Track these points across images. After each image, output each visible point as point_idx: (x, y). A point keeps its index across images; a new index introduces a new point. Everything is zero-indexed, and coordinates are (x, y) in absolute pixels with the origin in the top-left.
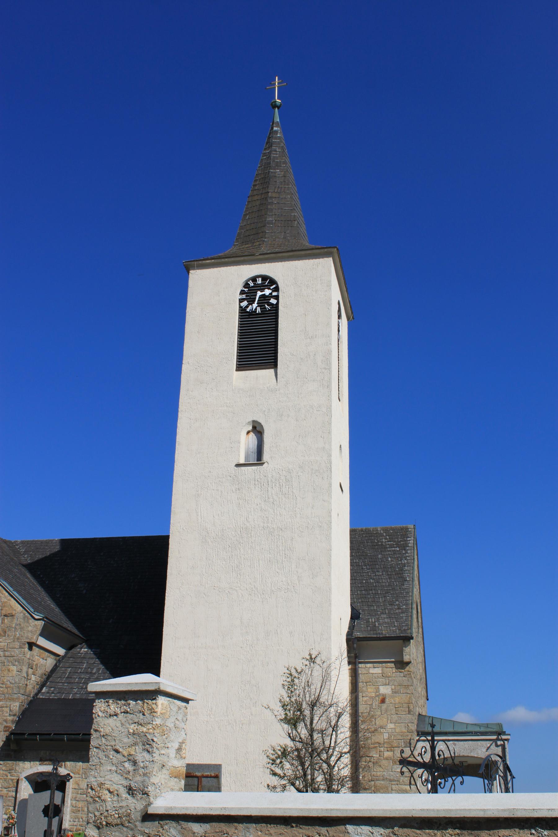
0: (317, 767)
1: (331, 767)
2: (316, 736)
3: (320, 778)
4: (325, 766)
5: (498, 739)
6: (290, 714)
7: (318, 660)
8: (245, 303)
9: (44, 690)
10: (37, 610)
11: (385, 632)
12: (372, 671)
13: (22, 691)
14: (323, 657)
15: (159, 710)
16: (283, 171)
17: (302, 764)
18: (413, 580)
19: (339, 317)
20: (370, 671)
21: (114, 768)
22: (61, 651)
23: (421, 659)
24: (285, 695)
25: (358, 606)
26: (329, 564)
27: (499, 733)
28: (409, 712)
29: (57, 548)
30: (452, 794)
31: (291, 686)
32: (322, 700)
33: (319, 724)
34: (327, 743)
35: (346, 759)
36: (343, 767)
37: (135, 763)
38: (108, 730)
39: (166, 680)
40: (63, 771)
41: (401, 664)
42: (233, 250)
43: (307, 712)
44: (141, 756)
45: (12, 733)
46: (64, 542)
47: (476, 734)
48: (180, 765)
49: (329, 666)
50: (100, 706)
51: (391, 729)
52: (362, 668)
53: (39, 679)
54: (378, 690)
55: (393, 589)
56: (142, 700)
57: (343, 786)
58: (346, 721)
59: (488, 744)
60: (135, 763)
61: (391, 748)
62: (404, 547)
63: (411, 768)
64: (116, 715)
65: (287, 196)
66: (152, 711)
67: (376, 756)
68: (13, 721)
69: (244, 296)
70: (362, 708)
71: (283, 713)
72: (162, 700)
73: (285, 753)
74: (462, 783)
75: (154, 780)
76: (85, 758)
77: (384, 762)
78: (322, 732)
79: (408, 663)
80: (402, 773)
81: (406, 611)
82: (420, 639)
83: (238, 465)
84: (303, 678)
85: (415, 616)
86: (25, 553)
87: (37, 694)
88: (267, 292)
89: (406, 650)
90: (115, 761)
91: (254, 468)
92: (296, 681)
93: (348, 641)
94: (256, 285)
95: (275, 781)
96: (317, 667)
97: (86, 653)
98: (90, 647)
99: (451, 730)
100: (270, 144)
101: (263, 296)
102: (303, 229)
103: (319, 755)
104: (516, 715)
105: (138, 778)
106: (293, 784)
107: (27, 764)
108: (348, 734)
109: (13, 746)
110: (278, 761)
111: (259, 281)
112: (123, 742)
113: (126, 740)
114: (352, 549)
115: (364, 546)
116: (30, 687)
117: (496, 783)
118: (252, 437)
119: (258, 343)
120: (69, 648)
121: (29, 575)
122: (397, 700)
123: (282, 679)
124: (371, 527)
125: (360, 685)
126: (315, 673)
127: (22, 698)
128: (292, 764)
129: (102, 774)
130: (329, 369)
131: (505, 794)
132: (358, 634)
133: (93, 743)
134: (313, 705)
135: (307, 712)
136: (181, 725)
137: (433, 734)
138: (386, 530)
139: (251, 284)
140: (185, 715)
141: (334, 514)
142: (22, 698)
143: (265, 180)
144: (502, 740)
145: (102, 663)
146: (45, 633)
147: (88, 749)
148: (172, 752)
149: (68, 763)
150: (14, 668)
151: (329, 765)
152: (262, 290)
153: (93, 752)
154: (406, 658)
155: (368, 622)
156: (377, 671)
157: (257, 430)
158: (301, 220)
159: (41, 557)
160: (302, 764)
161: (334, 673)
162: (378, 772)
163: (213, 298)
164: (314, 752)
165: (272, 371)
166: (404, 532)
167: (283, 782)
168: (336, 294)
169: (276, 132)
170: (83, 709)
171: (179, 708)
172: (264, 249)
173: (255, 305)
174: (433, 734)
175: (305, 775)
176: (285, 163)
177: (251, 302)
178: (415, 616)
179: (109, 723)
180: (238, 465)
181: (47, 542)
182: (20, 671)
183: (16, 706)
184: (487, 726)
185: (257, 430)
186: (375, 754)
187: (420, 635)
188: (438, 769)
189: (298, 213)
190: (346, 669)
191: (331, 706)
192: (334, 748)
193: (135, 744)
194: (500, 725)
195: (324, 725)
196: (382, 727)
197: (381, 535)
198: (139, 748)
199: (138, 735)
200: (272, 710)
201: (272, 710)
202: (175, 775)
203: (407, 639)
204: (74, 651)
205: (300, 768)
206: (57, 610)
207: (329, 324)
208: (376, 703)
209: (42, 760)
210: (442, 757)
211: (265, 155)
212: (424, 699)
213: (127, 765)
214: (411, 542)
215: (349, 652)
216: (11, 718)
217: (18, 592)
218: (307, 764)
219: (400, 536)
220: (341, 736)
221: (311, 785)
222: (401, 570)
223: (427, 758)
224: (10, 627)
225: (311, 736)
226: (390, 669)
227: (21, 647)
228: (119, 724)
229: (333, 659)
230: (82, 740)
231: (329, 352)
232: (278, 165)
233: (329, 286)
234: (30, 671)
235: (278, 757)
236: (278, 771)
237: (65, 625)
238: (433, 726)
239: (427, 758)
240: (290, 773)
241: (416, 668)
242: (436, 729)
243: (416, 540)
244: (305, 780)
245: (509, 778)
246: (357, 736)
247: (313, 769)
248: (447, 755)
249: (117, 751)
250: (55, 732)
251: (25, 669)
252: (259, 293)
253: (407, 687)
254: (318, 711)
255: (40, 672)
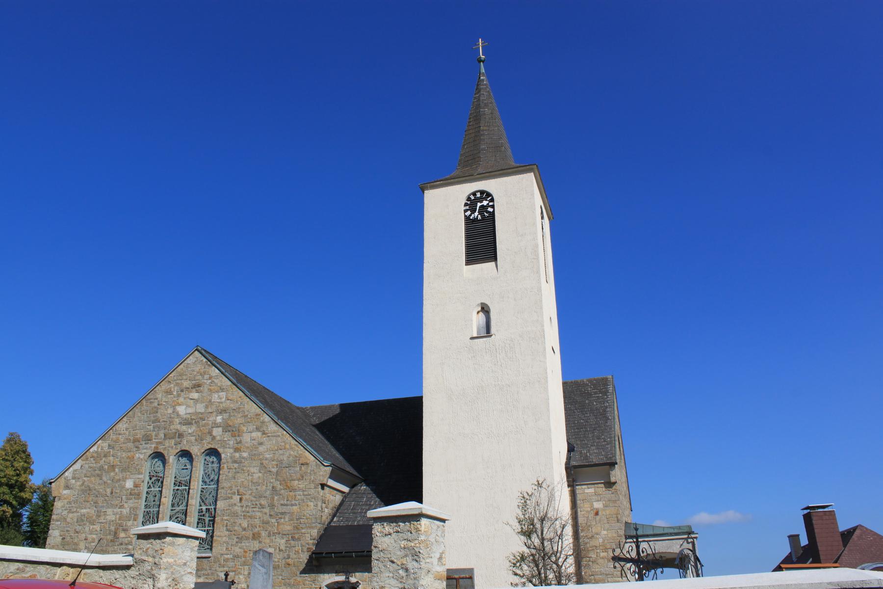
0: (548, 567)
1: (559, 567)
2: (546, 543)
3: (551, 576)
4: (554, 566)
5: (688, 538)
6: (525, 528)
7: (544, 485)
8: (469, 213)
9: (335, 519)
10: (325, 459)
11: (595, 460)
12: (587, 491)
13: (319, 521)
14: (548, 482)
15: (423, 529)
16: (491, 109)
17: (537, 566)
18: (614, 418)
19: (542, 218)
20: (586, 491)
21: (391, 575)
22: (346, 489)
23: (624, 479)
24: (520, 513)
25: (572, 441)
26: (548, 410)
27: (689, 533)
28: (618, 521)
29: (338, 411)
30: (655, 581)
31: (524, 506)
32: (549, 515)
33: (548, 534)
34: (555, 548)
35: (571, 560)
36: (569, 567)
37: (407, 570)
38: (385, 546)
39: (426, 507)
40: (353, 580)
41: (609, 484)
42: (455, 173)
43: (538, 526)
44: (411, 565)
45: (313, 553)
46: (343, 407)
47: (671, 534)
48: (442, 570)
49: (553, 489)
50: (377, 528)
51: (605, 535)
52: (579, 489)
53: (331, 511)
54: (592, 505)
55: (599, 427)
56: (409, 522)
57: (570, 581)
58: (569, 531)
59: (681, 542)
60: (407, 570)
61: (605, 550)
62: (606, 393)
63: (622, 563)
64: (390, 534)
65: (495, 127)
66: (418, 530)
67: (594, 556)
68: (313, 544)
69: (467, 207)
70: (581, 520)
71: (519, 527)
72: (424, 521)
73: (523, 558)
74: (662, 572)
75: (422, 582)
76: (369, 569)
77: (600, 561)
78: (551, 540)
79: (615, 483)
80: (615, 567)
81: (610, 442)
82: (623, 464)
83: (472, 338)
84: (534, 499)
85: (617, 446)
86: (314, 416)
87: (330, 523)
88: (485, 203)
89: (613, 473)
90: (391, 569)
91: (484, 339)
92: (528, 502)
93: (566, 469)
94: (476, 199)
95: (516, 579)
96: (543, 490)
97: (365, 490)
98: (367, 485)
99: (652, 533)
100: (478, 90)
101: (482, 206)
102: (509, 152)
103: (549, 558)
104: (700, 519)
105: (411, 582)
106: (531, 582)
107: (326, 576)
108: (571, 540)
109: (315, 563)
110: (518, 564)
111: (478, 195)
112: (397, 555)
113: (399, 553)
114: (565, 397)
115: (575, 395)
116: (324, 518)
117: (689, 572)
118: (482, 316)
119: (481, 242)
120: (352, 486)
121: (318, 433)
122: (608, 512)
123: (517, 502)
124: (579, 379)
125: (578, 502)
126: (543, 495)
127: (319, 526)
128: (529, 566)
129: (382, 579)
130: (537, 258)
131: (696, 579)
132: (574, 463)
133: (374, 556)
134: (542, 520)
135: (538, 526)
136: (441, 539)
137: (637, 537)
138: (590, 381)
139: (472, 198)
140: (443, 532)
141: (549, 371)
142: (319, 526)
143: (477, 117)
144: (693, 538)
145: (378, 497)
146: (333, 476)
147: (370, 562)
148: (435, 561)
149: (357, 574)
150: (312, 504)
151: (558, 565)
152: (481, 202)
153: (374, 563)
154: (613, 480)
155: (581, 453)
156: (590, 490)
157: (485, 309)
158: (507, 146)
159: (326, 418)
160: (537, 566)
161: (557, 494)
162: (596, 568)
163: (444, 211)
164: (545, 556)
165: (493, 263)
166: (604, 382)
167: (523, 580)
168: (538, 201)
169: (483, 80)
170: (364, 533)
171: (438, 527)
172: (480, 170)
173: (476, 214)
174: (637, 537)
175: (540, 574)
176: (491, 103)
177: (473, 211)
178: (617, 446)
179: (384, 540)
180: (472, 338)
181: (330, 407)
182: (316, 506)
183: (315, 533)
184: (680, 528)
185: (485, 309)
186: (593, 555)
187: (623, 461)
188: (643, 562)
189: (505, 141)
190: (566, 491)
191: (556, 520)
192: (561, 552)
193: (406, 556)
194: (690, 527)
195: (552, 535)
196: (597, 534)
197: (587, 385)
198: (409, 559)
199: (408, 548)
200: (511, 526)
201: (511, 526)
202: (438, 578)
203: (613, 465)
204: (355, 488)
205: (535, 569)
206: (341, 458)
207: (535, 224)
208: (592, 515)
209: (337, 572)
210: (645, 553)
211: (475, 98)
212: (629, 510)
213: (401, 572)
214: (611, 389)
215: (568, 477)
216: (311, 542)
217: (311, 446)
218: (541, 565)
219: (602, 386)
220: (566, 543)
221: (545, 581)
222: (604, 411)
223: (634, 554)
224: (306, 473)
225: (543, 543)
226: (601, 489)
227: (315, 488)
228: (393, 541)
229: (556, 483)
230: (367, 556)
231: (537, 246)
232: (486, 105)
233: (533, 194)
234: (324, 505)
235: (518, 561)
236: (519, 572)
237: (348, 469)
238: (636, 529)
239: (634, 554)
240: (527, 573)
241: (621, 486)
242: (640, 532)
243: (614, 387)
244: (540, 578)
245: (699, 566)
246: (578, 542)
247: (546, 569)
248: (649, 552)
249: (393, 562)
250: (343, 550)
251: (319, 504)
252: (479, 204)
253: (615, 501)
254: (547, 524)
255: (331, 505)
